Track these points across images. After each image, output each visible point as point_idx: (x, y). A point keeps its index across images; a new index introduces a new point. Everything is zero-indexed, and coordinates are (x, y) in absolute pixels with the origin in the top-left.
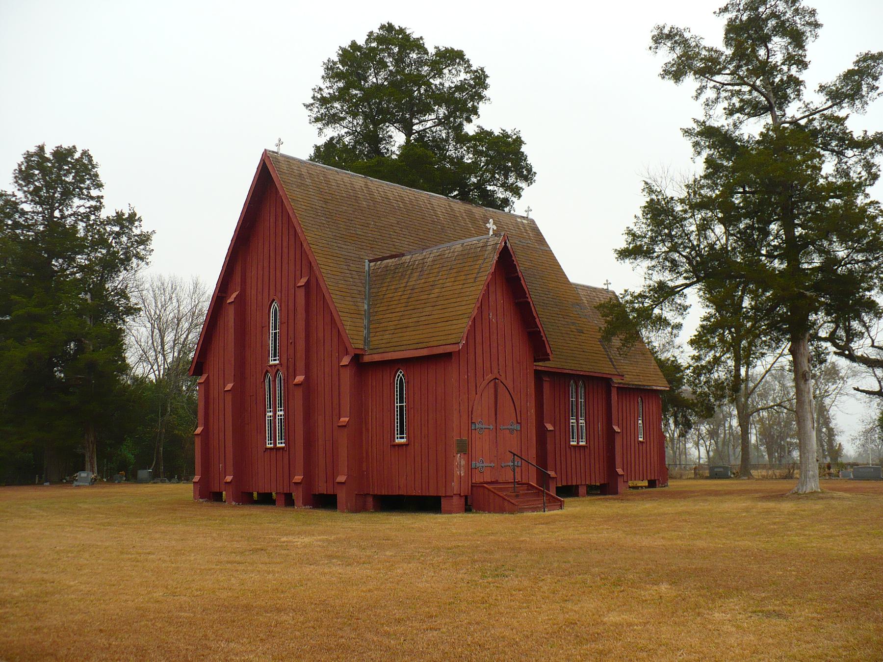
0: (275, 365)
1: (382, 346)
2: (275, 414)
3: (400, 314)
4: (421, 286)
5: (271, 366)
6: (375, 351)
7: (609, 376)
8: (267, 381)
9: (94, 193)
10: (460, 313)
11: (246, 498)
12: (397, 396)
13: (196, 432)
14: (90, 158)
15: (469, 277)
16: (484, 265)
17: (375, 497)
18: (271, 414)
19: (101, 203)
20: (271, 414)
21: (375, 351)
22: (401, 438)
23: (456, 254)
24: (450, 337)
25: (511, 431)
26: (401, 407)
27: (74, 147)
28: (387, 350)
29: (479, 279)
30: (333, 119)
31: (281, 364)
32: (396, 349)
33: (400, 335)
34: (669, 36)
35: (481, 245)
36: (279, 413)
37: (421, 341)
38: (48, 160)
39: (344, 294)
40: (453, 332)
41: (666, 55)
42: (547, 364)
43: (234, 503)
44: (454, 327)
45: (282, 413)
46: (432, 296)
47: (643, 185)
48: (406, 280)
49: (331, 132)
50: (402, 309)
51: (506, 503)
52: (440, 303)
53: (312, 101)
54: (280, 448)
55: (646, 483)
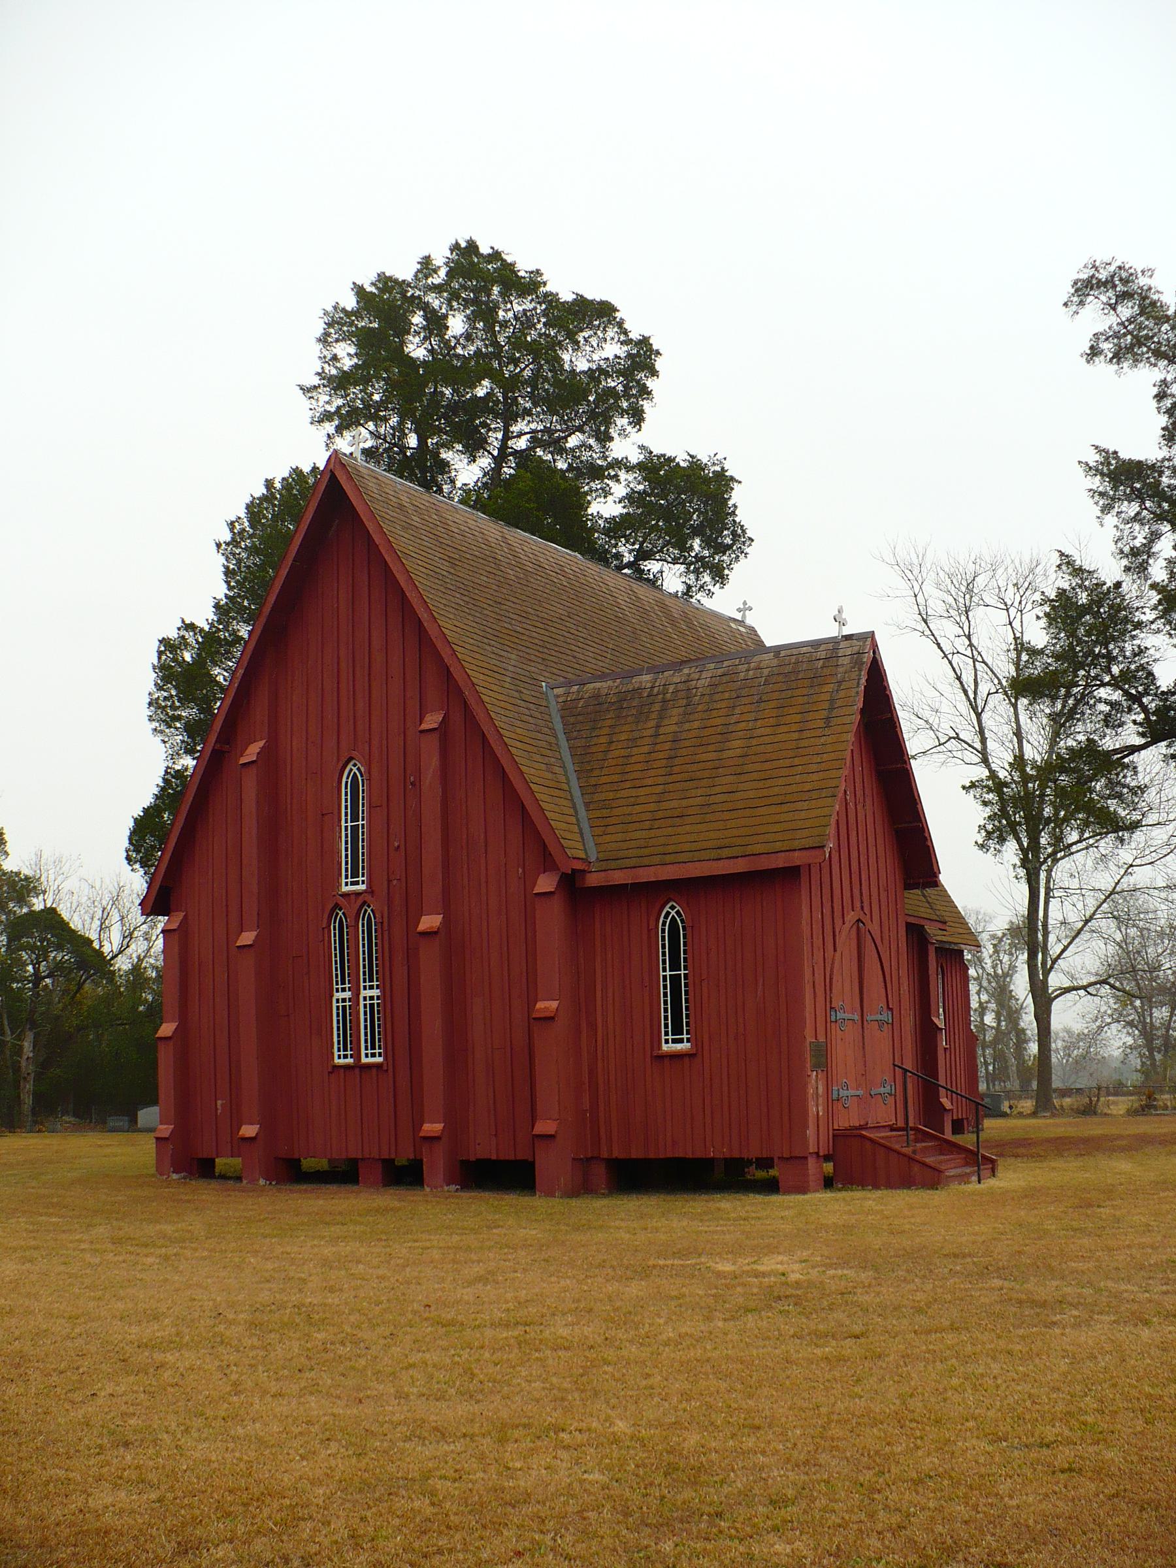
0: (358, 894)
1: (631, 853)
3: (659, 789)
4: (694, 733)
5: (346, 895)
6: (613, 865)
7: (922, 922)
10: (808, 787)
11: (290, 1172)
13: (160, 1033)
15: (811, 716)
16: (842, 694)
18: (347, 995)
20: (347, 995)
21: (613, 865)
23: (766, 672)
24: (799, 834)
25: (880, 1024)
26: (675, 980)
28: (646, 861)
29: (662, 730)
30: (347, 420)
31: (370, 891)
32: (668, 858)
33: (670, 831)
34: (1108, 283)
35: (823, 655)
36: (364, 993)
37: (726, 842)
39: (529, 748)
40: (800, 824)
41: (1096, 318)
43: (262, 1182)
44: (803, 815)
46: (730, 753)
48: (652, 723)
50: (661, 780)
51: (916, 1168)
52: (751, 767)
53: (316, 381)
54: (369, 1066)
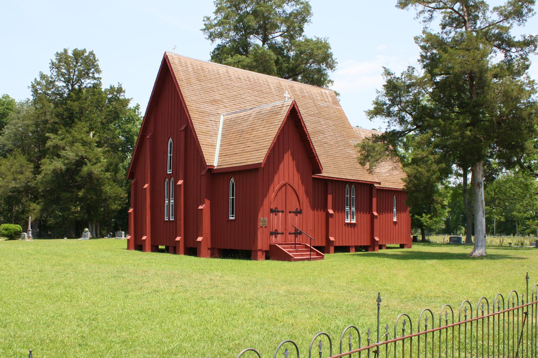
2: (169, 202)
8: (166, 183)
9: (96, 75)
12: (231, 193)
14: (94, 55)
17: (219, 249)
19: (100, 82)
22: (233, 216)
27: (85, 50)
38: (70, 57)
42: (321, 175)
45: (173, 201)
47: (383, 70)
49: (219, 41)
55: (398, 246)
